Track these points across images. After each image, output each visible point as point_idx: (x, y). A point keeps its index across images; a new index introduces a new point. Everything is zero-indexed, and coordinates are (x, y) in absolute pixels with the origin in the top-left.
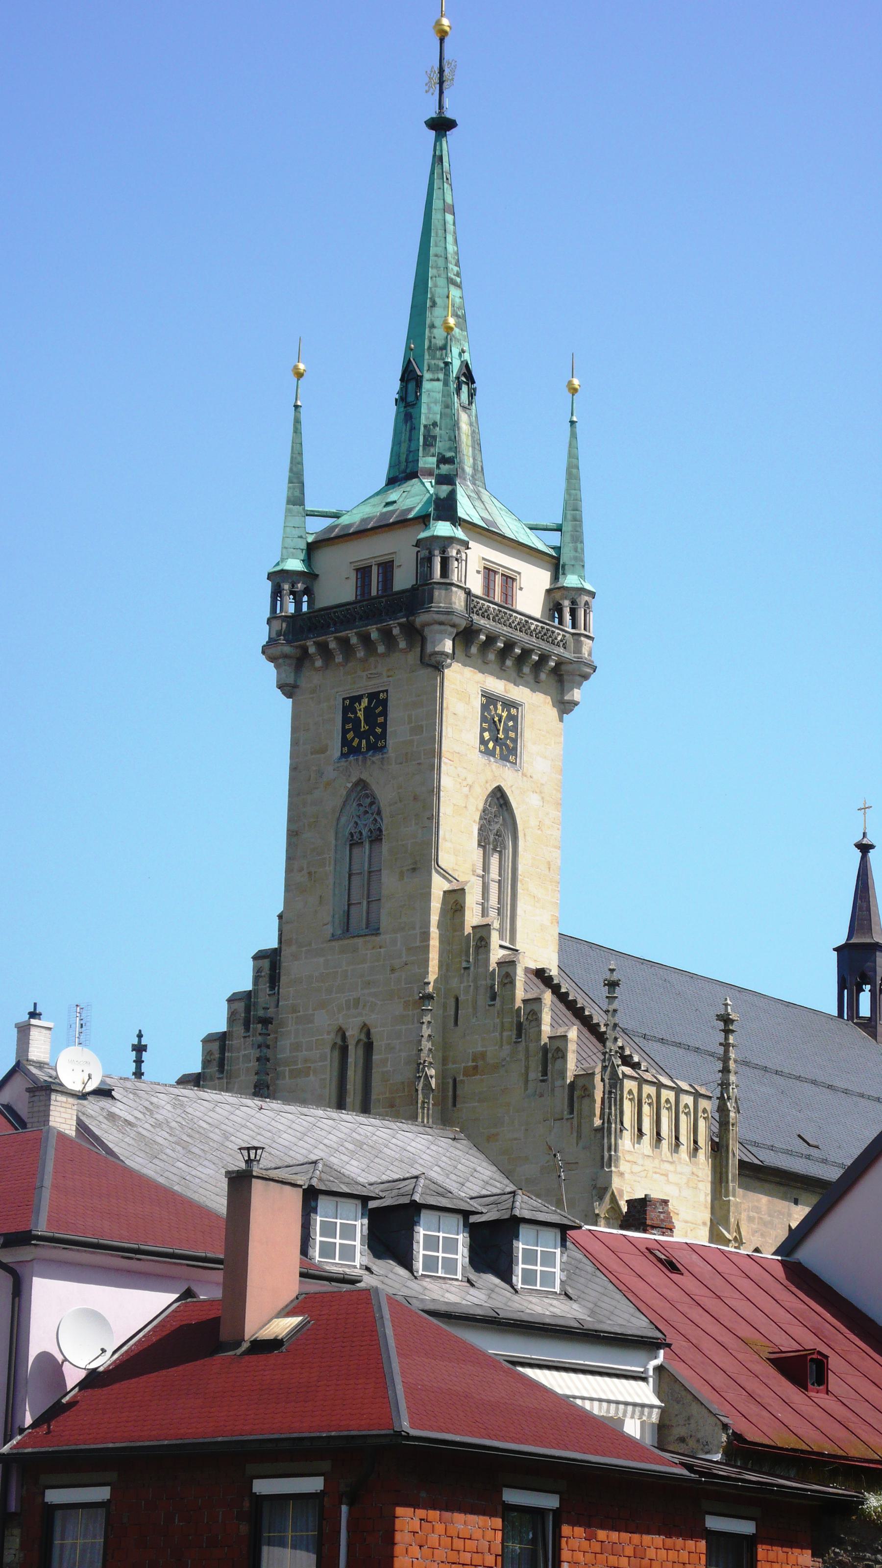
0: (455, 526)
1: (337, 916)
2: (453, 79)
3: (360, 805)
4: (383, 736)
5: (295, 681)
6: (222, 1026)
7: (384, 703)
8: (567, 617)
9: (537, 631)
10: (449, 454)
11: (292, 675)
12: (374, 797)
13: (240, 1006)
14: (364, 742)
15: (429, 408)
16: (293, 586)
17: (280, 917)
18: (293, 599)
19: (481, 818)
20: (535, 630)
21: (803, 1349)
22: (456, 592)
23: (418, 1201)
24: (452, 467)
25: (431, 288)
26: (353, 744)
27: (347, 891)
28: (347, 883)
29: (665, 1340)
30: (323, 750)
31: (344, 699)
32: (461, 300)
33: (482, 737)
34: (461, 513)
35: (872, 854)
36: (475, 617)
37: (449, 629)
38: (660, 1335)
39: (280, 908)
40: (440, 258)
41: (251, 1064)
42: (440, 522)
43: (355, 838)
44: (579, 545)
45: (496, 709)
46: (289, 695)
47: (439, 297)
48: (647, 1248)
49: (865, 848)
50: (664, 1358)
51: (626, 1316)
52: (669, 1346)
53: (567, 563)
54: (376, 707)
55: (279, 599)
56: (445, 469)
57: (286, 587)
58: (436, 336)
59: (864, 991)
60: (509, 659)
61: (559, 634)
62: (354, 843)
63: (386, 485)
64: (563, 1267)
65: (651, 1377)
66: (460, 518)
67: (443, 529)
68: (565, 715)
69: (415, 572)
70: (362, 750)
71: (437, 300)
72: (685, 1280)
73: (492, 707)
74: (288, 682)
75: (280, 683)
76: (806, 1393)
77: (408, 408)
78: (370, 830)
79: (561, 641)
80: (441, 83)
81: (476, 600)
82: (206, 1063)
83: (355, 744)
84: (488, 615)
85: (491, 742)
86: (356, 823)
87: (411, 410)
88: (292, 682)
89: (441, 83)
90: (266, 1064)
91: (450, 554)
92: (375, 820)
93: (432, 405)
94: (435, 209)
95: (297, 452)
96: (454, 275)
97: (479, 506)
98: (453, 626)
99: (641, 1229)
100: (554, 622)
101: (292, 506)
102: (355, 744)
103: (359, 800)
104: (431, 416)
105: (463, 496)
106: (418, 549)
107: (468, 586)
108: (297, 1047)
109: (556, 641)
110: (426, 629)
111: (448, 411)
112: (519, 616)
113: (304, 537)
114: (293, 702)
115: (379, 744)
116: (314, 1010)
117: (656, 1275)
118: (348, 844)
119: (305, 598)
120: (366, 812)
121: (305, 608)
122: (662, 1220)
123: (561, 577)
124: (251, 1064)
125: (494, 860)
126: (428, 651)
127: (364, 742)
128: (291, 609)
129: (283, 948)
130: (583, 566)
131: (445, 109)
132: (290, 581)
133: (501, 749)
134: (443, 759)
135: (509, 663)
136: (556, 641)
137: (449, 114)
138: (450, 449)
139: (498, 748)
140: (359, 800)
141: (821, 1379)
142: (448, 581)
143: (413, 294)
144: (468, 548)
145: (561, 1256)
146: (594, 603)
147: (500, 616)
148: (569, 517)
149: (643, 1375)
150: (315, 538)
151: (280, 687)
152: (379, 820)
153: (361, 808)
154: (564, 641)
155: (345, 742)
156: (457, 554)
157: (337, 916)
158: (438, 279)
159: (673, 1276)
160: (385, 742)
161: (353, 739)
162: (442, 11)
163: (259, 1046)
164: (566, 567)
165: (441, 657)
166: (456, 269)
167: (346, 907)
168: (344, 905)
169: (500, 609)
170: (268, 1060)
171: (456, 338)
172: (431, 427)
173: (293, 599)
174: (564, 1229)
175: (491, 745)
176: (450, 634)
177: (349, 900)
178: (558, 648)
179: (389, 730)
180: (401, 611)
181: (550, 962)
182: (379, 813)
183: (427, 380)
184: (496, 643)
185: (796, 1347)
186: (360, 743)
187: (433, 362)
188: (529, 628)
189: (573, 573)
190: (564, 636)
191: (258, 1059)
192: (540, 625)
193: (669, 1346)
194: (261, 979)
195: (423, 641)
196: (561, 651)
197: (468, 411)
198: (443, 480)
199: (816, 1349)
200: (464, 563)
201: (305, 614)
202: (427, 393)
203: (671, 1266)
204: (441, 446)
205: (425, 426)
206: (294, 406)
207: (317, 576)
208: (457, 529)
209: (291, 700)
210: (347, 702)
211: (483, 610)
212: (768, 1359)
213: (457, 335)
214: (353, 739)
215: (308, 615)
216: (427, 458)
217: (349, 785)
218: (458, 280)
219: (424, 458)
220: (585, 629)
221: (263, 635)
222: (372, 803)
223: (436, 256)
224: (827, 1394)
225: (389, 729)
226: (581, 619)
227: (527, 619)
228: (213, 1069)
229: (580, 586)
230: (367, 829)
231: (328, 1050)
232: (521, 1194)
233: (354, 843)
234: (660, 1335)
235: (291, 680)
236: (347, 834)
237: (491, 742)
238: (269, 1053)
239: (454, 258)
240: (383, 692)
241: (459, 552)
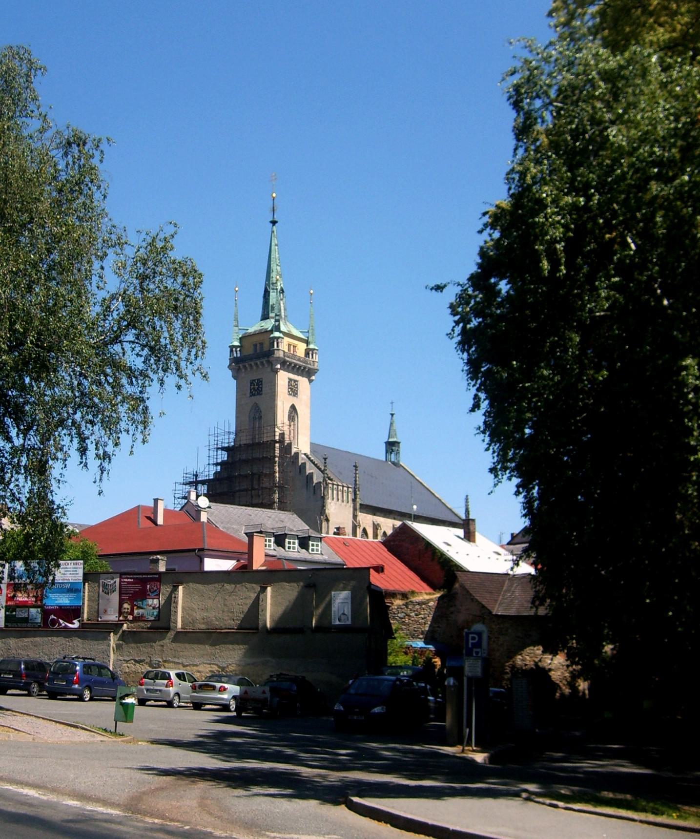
7: (262, 382)
56: (277, 318)
62: (254, 418)
72: (350, 548)
80: (274, 211)
89: (274, 211)
117: (342, 546)
155: (251, 392)
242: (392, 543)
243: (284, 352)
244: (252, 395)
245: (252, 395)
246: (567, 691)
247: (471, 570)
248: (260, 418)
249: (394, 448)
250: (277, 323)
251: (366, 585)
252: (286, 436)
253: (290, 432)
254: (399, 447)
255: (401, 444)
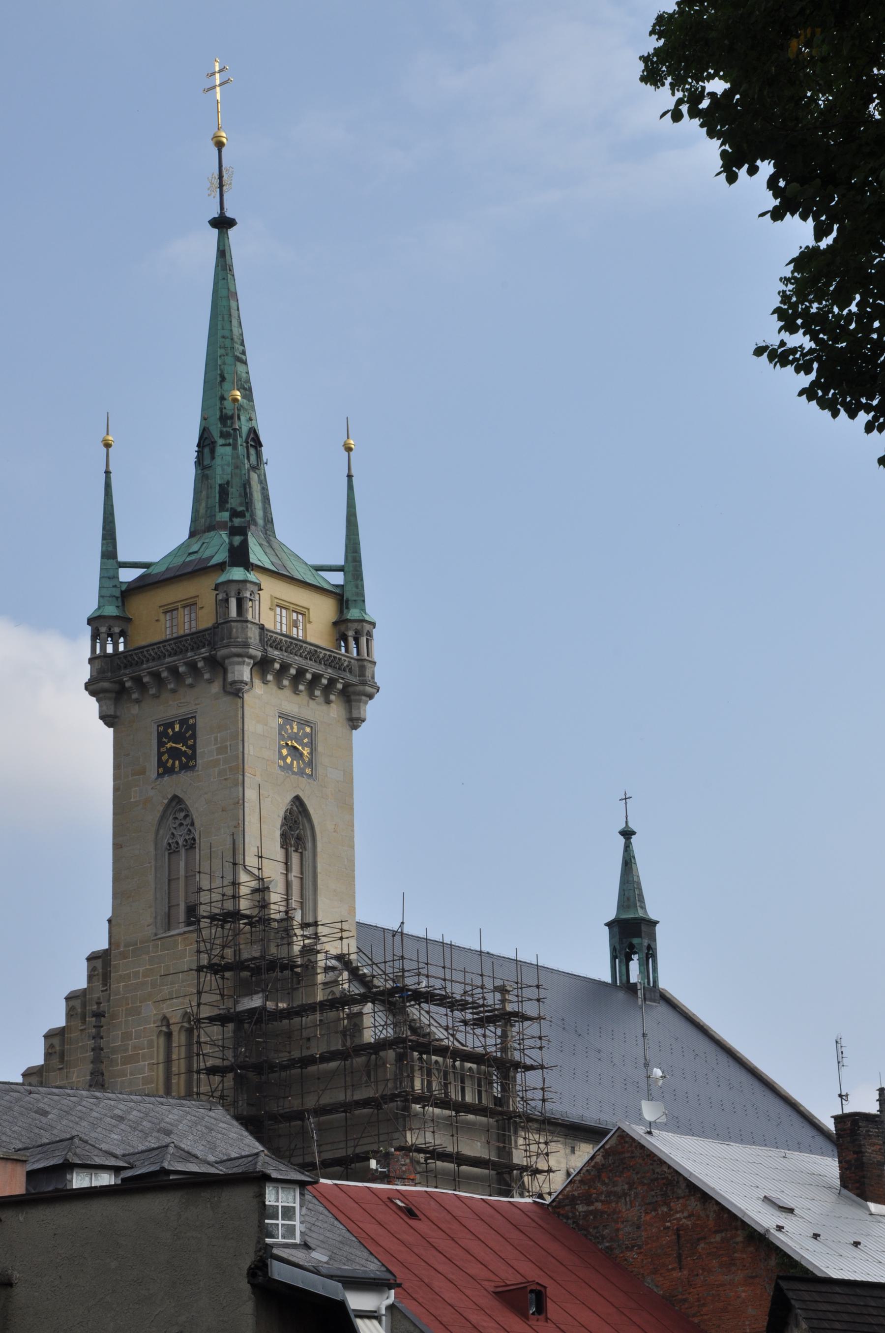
0: (248, 571)
1: (159, 918)
2: (230, 184)
3: (176, 818)
4: (193, 757)
5: (115, 712)
6: (60, 1021)
7: (193, 727)
8: (352, 644)
9: (326, 659)
10: (240, 509)
11: (112, 707)
12: (186, 809)
13: (77, 1003)
14: (177, 763)
15: (223, 470)
16: (110, 629)
17: (109, 921)
18: (111, 641)
19: (282, 826)
20: (323, 658)
21: (526, 1281)
22: (251, 628)
23: (166, 1167)
24: (243, 520)
25: (220, 366)
26: (168, 765)
27: (167, 895)
28: (167, 887)
29: (396, 1281)
30: (143, 772)
31: (158, 726)
32: (247, 375)
33: (280, 753)
34: (253, 559)
35: (634, 839)
36: (269, 649)
37: (247, 660)
38: (389, 1276)
39: (109, 914)
40: (227, 340)
41: (88, 1054)
42: (235, 569)
43: (172, 847)
44: (360, 583)
45: (292, 728)
46: (109, 725)
47: (227, 373)
48: (388, 1198)
49: (627, 834)
50: (395, 1297)
51: (363, 1262)
52: (399, 1286)
53: (350, 598)
54: (186, 731)
55: (98, 641)
56: (237, 521)
57: (103, 629)
58: (226, 407)
59: (633, 960)
60: (318, 689)
61: (345, 661)
62: (172, 850)
63: (189, 538)
64: (303, 1219)
65: (383, 1315)
66: (252, 564)
67: (237, 573)
68: (354, 731)
69: (215, 612)
70: (176, 770)
71: (226, 375)
72: (421, 1226)
73: (288, 727)
74: (109, 714)
75: (102, 714)
76: (527, 1322)
77: (205, 470)
78: (186, 840)
79: (348, 666)
80: (221, 186)
81: (270, 634)
82: (48, 1055)
83: (169, 764)
84: (281, 647)
85: (289, 758)
86: (173, 834)
87: (207, 472)
88: (112, 713)
89: (221, 186)
90: (100, 1054)
91: (245, 595)
92: (189, 830)
93: (225, 467)
94: (221, 297)
95: (109, 513)
96: (240, 353)
97: (269, 552)
98: (250, 657)
99: (386, 1181)
100: (341, 650)
101: (106, 560)
102: (169, 764)
103: (175, 813)
104: (225, 477)
105: (255, 545)
106: (217, 592)
107: (262, 622)
108: (127, 1036)
109: (343, 667)
110: (227, 661)
111: (238, 471)
112: (324, 652)
113: (118, 586)
114: (114, 732)
115: (191, 764)
116: (140, 1003)
117: (396, 1223)
118: (167, 853)
119: (122, 640)
120: (181, 824)
121: (121, 648)
122: (404, 1172)
123: (345, 611)
124: (88, 1054)
125: (295, 858)
126: (229, 680)
127: (177, 763)
128: (110, 649)
129: (113, 948)
130: (364, 601)
131: (225, 210)
132: (107, 625)
133: (298, 763)
134: (246, 774)
135: (317, 693)
136: (343, 667)
137: (229, 214)
138: (241, 505)
139: (295, 762)
140: (175, 813)
141: (541, 1309)
142: (243, 619)
143: (205, 371)
144: (260, 589)
145: (301, 1209)
146: (375, 632)
147: (292, 647)
148: (350, 559)
149: (376, 1314)
150: (127, 587)
151: (102, 717)
152: (193, 830)
153: (177, 821)
154: (350, 667)
155: (161, 763)
156: (251, 595)
157: (159, 918)
158: (226, 357)
159: (412, 1222)
160: (196, 762)
161: (167, 760)
162: (219, 125)
163: (94, 1038)
164: (350, 602)
165: (241, 685)
166: (241, 348)
167: (167, 909)
168: (165, 908)
169: (292, 641)
170: (102, 1049)
171: (244, 408)
172: (226, 486)
173: (111, 641)
174: (302, 1184)
175: (289, 760)
176: (248, 664)
177: (169, 903)
178: (344, 673)
179: (198, 751)
180: (204, 647)
181: (350, 946)
182: (192, 824)
183: (221, 446)
184: (289, 670)
185: (520, 1279)
186: (174, 764)
187: (225, 429)
188: (318, 657)
189: (355, 607)
190: (350, 662)
191: (93, 1050)
192: (328, 653)
193: (399, 1286)
194: (94, 978)
195: (225, 671)
196: (347, 675)
197: (257, 471)
198: (235, 531)
199: (534, 1281)
200: (257, 603)
201: (122, 653)
202: (221, 457)
203: (410, 1212)
204: (234, 502)
205: (220, 485)
206: (105, 472)
207: (131, 619)
208: (250, 574)
209: (112, 729)
210: (161, 728)
211: (276, 643)
212: (494, 1292)
213: (245, 405)
214: (167, 760)
215: (124, 654)
216: (223, 513)
217: (166, 801)
218: (244, 357)
219: (220, 514)
220: (368, 655)
221: (85, 673)
222: (186, 816)
223: (223, 337)
224: (547, 1321)
225: (199, 751)
226: (363, 648)
227: (316, 649)
228: (55, 1061)
229: (361, 618)
230: (182, 839)
231: (155, 1038)
232: (263, 1155)
233: (172, 850)
234: (389, 1276)
235: (111, 712)
236: (165, 844)
237: (289, 758)
238: (102, 1043)
239: (239, 339)
240: (192, 718)
241: (252, 593)
242: (581, 1208)
243: (262, 627)
244: (165, 770)
245: (165, 770)
246: (790, 287)
247: (157, 561)
248: (191, 845)
249: (635, 941)
250: (237, 540)
251: (246, 1262)
252: (275, 897)
253: (288, 885)
254: (653, 937)
255: (658, 928)
